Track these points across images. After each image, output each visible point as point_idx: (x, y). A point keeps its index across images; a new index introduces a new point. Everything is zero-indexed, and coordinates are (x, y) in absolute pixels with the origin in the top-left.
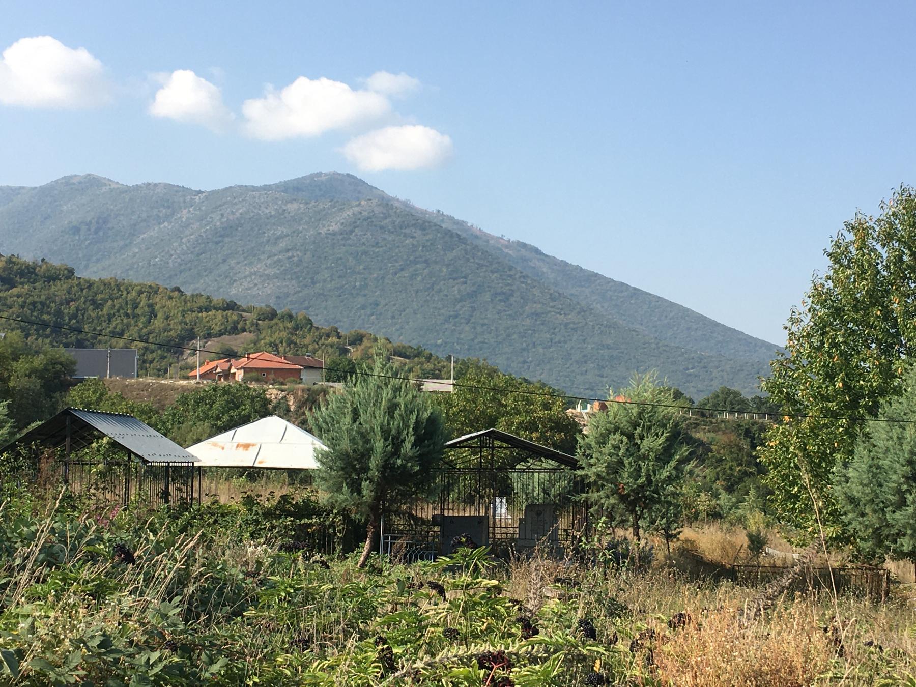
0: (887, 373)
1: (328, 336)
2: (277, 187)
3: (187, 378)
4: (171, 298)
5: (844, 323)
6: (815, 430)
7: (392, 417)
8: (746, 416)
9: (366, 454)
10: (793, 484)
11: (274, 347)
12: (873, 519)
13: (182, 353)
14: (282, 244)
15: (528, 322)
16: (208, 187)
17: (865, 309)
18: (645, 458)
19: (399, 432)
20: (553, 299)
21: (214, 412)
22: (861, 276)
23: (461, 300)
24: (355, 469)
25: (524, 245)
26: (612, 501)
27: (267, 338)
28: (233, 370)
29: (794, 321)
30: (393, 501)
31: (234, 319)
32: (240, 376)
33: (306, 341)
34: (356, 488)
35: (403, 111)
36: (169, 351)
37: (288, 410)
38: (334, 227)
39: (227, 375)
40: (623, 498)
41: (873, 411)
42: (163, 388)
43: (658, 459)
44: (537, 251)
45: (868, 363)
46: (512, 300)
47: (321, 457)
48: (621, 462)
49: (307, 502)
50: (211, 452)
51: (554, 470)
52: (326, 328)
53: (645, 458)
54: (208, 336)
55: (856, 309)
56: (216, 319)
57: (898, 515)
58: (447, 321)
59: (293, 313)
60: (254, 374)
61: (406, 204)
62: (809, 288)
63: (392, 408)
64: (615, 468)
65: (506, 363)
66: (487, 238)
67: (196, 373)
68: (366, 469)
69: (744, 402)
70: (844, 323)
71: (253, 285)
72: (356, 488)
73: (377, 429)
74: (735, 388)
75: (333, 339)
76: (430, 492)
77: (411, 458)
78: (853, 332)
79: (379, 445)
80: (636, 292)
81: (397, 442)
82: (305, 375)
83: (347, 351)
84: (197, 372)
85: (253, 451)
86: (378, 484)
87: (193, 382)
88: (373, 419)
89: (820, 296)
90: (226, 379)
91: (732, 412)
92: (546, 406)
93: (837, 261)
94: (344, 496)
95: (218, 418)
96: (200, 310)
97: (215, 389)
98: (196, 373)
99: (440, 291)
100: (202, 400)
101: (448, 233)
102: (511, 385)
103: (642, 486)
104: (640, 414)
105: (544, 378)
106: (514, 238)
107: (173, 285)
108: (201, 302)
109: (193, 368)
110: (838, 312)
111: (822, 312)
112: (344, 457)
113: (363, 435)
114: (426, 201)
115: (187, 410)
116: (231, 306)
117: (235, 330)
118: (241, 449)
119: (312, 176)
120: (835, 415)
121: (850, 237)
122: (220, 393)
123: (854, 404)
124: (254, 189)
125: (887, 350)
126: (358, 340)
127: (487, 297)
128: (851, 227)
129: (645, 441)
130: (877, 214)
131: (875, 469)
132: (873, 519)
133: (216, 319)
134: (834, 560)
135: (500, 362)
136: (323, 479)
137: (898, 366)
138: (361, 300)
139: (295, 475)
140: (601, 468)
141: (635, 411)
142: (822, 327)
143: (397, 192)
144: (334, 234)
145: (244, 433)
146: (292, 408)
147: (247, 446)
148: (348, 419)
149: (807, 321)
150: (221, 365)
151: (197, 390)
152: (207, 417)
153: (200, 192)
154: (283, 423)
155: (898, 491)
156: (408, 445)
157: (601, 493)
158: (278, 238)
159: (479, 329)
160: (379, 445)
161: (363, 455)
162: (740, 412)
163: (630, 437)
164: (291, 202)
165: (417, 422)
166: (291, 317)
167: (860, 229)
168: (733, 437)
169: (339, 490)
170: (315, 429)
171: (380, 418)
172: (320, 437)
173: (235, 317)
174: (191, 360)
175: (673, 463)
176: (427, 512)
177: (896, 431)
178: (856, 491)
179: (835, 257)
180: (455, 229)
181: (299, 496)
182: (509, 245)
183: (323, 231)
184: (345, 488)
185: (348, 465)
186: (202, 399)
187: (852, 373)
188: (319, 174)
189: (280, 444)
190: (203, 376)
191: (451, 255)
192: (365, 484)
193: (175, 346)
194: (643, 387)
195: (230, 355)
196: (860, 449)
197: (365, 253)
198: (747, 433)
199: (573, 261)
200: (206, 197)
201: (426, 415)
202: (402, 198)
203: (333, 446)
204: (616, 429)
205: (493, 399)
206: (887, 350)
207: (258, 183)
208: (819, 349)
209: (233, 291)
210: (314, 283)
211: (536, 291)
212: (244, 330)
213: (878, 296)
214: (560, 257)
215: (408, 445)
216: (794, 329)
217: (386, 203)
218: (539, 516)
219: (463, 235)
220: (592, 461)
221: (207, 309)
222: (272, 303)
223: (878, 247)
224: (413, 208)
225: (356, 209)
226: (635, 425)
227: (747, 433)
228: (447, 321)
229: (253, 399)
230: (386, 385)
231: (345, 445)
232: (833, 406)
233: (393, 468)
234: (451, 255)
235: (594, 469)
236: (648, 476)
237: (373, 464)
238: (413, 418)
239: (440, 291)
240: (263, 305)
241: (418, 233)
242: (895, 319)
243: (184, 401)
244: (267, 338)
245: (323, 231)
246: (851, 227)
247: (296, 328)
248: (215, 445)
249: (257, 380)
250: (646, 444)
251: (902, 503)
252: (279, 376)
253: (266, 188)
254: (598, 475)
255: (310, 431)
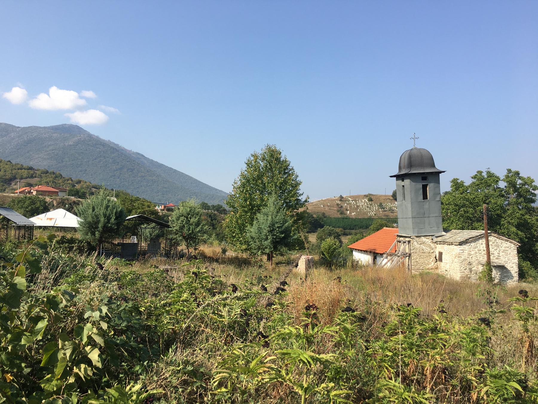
0: (262, 200)
1: (68, 180)
2: (49, 128)
3: (14, 193)
4: (7, 164)
5: (250, 184)
6: (241, 216)
7: (107, 210)
8: (210, 211)
9: (98, 222)
10: (233, 233)
11: (47, 183)
12: (258, 243)
13: (11, 184)
14: (51, 148)
15: (139, 179)
16: (22, 126)
17: (256, 181)
18: (192, 224)
19: (110, 215)
20: (148, 172)
21: (25, 205)
22: (255, 170)
23: (117, 170)
24: (93, 227)
25: (139, 154)
26: (181, 238)
27: (44, 180)
28: (32, 191)
29: (235, 183)
30: (106, 238)
31: (32, 173)
32: (35, 193)
33: (60, 182)
34: (93, 234)
35: (91, 105)
36: (5, 183)
37: (54, 205)
38: (71, 143)
39: (30, 192)
40: (184, 237)
41: (259, 210)
42: (4, 196)
43: (196, 225)
44: (143, 156)
45: (257, 195)
46: (134, 171)
47: (81, 224)
48: (184, 226)
49: (72, 238)
50: (39, 220)
51: (154, 228)
52: (67, 178)
53: (192, 224)
54: (21, 179)
55: (253, 180)
56: (25, 173)
57: (265, 242)
58: (111, 177)
59: (55, 172)
60: (40, 193)
61: (97, 137)
62: (240, 173)
63: (107, 207)
64: (182, 228)
65: (133, 192)
66: (126, 150)
67: (18, 191)
68: (98, 227)
69: (209, 206)
70: (250, 184)
71: (40, 161)
72: (93, 234)
73: (102, 214)
74: (206, 202)
75: (70, 182)
76: (120, 235)
77: (113, 224)
78: (252, 187)
79: (102, 219)
80: (175, 171)
81: (109, 219)
82: (59, 194)
83: (75, 186)
84: (18, 191)
85: (53, 221)
86: (101, 233)
87: (16, 194)
88: (101, 211)
89: (242, 175)
90: (29, 194)
91: (205, 209)
92: (149, 207)
93: (248, 165)
94: (89, 237)
95: (27, 208)
96: (18, 169)
97: (26, 198)
98: (18, 191)
99: (109, 167)
100: (20, 201)
101: (112, 147)
102: (137, 199)
103: (190, 234)
104: (190, 211)
105: (144, 197)
106: (135, 151)
107: (7, 160)
108: (19, 166)
109: (15, 190)
110: (248, 181)
111: (244, 181)
112: (89, 223)
113: (96, 216)
114: (104, 136)
115: (14, 205)
116: (31, 168)
117: (32, 177)
118: (49, 220)
119: (63, 125)
120: (246, 212)
121: (252, 158)
122: (27, 199)
123: (252, 209)
124: (40, 128)
125: (262, 193)
126: (79, 182)
127: (125, 170)
128: (252, 156)
129: (192, 219)
130: (261, 152)
131: (260, 229)
132: (258, 243)
133: (25, 173)
134: (245, 256)
135: (129, 191)
136: (81, 231)
137: (265, 198)
138: (80, 168)
139: (74, 229)
140: (177, 228)
141: (189, 210)
142: (243, 185)
143: (92, 132)
144: (71, 145)
145: (49, 214)
146: (55, 205)
147: (51, 219)
148: (91, 210)
149: (239, 183)
150: (27, 189)
151: (18, 198)
152: (22, 207)
153: (19, 127)
154: (65, 211)
155: (266, 235)
156: (113, 219)
157: (177, 236)
158: (50, 145)
159: (122, 180)
160: (102, 219)
161: (96, 223)
162: (208, 209)
163: (187, 218)
164: (55, 133)
165: (116, 213)
166: (54, 173)
167: (255, 156)
168: (206, 217)
169: (87, 234)
170: (78, 215)
171: (103, 211)
172: (80, 217)
173: (32, 172)
174: (15, 187)
175: (200, 226)
176: (116, 242)
177: (266, 217)
178: (253, 235)
179: (248, 164)
180: (113, 146)
181: (69, 236)
182: (134, 153)
183: (66, 144)
184: (89, 234)
185: (91, 226)
186: (20, 201)
187: (252, 199)
188: (65, 124)
189: (62, 218)
190: (20, 192)
191: (113, 155)
192: (97, 233)
193: (9, 181)
194: (193, 202)
195: (30, 185)
196: (255, 222)
197: (82, 153)
198: (210, 216)
199: (155, 159)
200: (21, 129)
201: (119, 210)
202: (96, 135)
203: (85, 220)
204: (182, 216)
205: (131, 204)
206: (262, 193)
207: (42, 126)
208: (242, 192)
209: (31, 163)
210: (62, 162)
211: (142, 169)
212: (36, 177)
213: (260, 177)
214: (151, 158)
215: (113, 219)
216: (235, 185)
217: (90, 136)
218: (154, 241)
219: (118, 149)
220: (174, 225)
221: (21, 169)
222: (46, 168)
223: (260, 162)
224: (100, 139)
225: (79, 138)
226: (189, 214)
227: (210, 216)
228: (111, 177)
229: (40, 201)
230: (105, 199)
231: (90, 219)
232: (246, 209)
233: (107, 227)
234: (113, 155)
235: (175, 228)
236: (192, 230)
237: (100, 225)
238: (115, 211)
239: (109, 167)
240: (43, 169)
241: (102, 147)
242: (265, 184)
243: (13, 201)
244: (44, 180)
245: (66, 144)
246: (252, 156)
247: (56, 177)
248: (39, 218)
249: (42, 195)
250: (192, 220)
251: (267, 239)
252: (50, 193)
253: (45, 128)
254: (176, 230)
255: (76, 215)
